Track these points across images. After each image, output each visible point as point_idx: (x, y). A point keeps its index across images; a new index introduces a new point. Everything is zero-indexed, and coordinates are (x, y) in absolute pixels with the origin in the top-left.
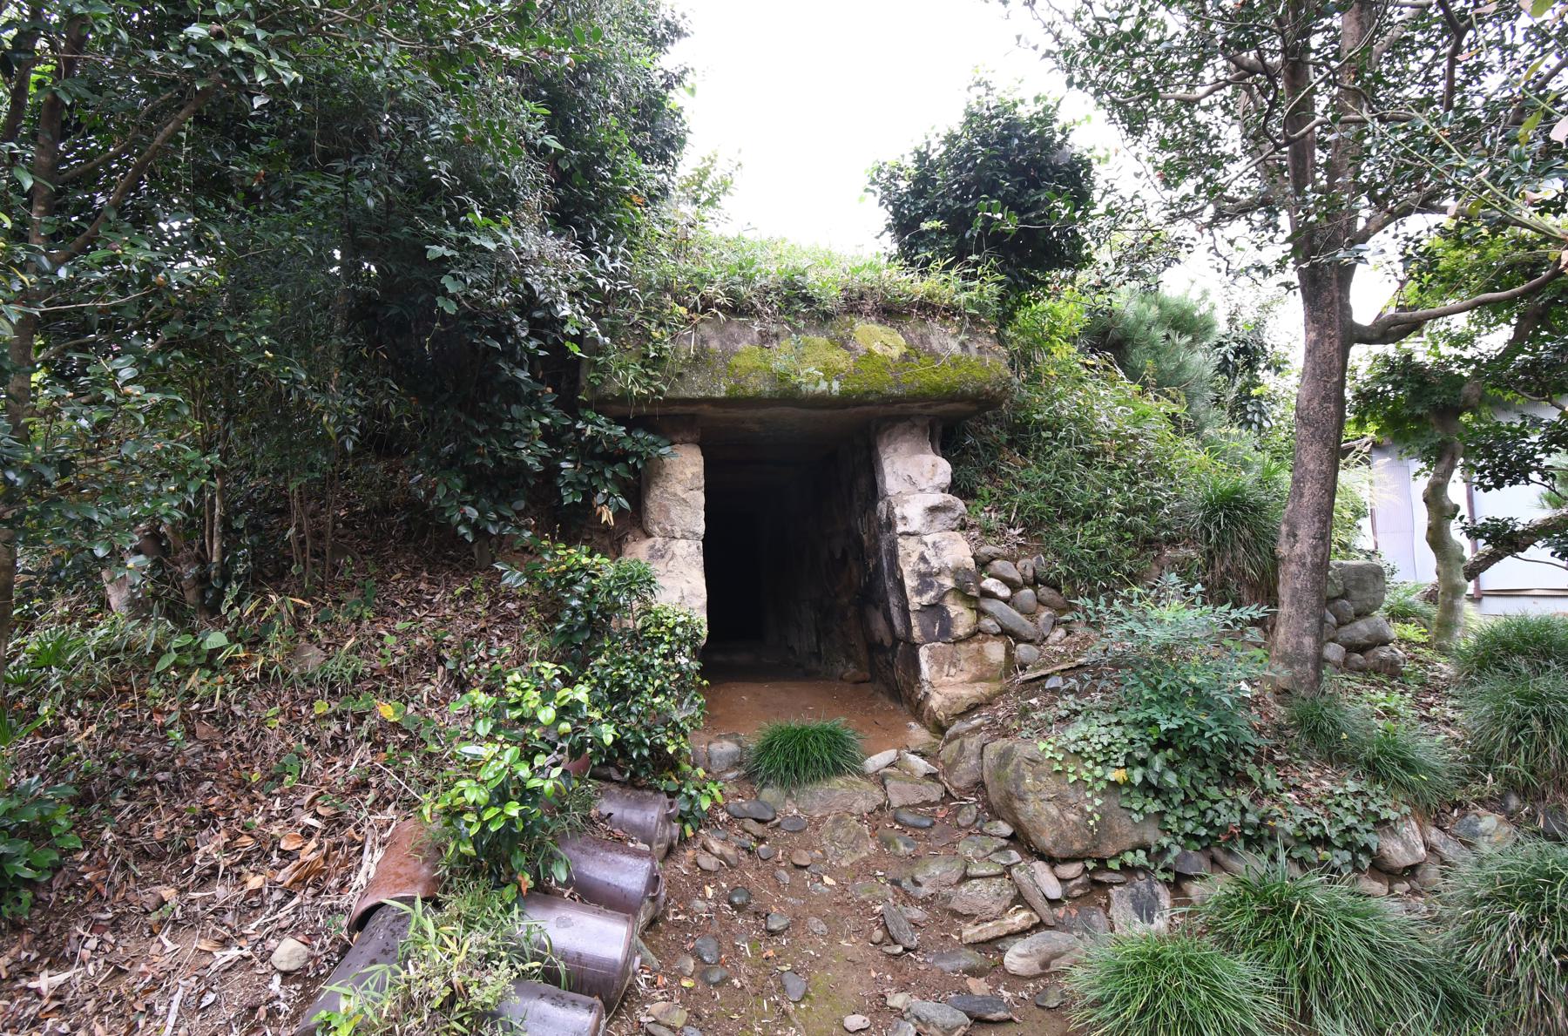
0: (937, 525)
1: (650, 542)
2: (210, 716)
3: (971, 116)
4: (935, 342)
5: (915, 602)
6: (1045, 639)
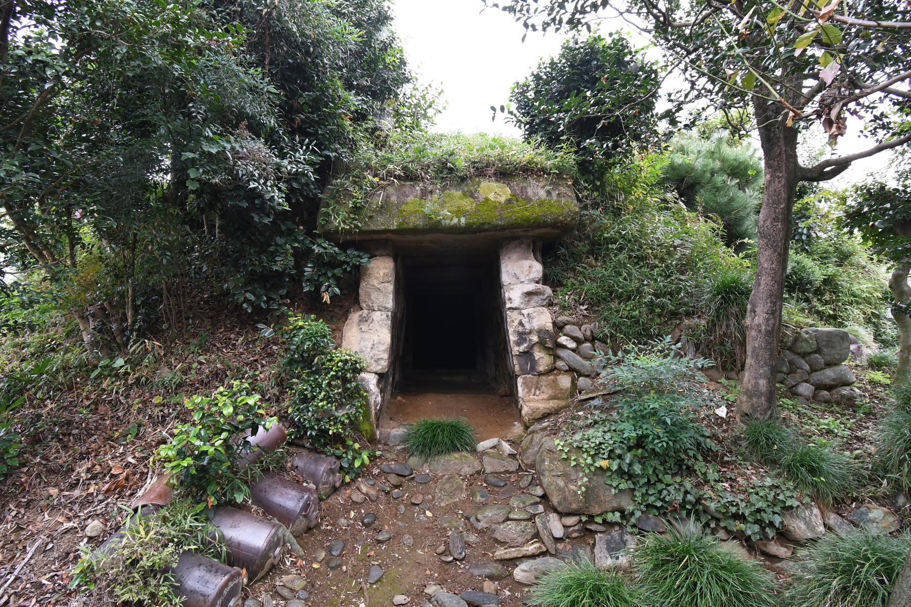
0: (533, 303)
1: (361, 313)
2: (110, 402)
3: (566, 48)
4: (530, 192)
5: (516, 350)
6: (598, 375)
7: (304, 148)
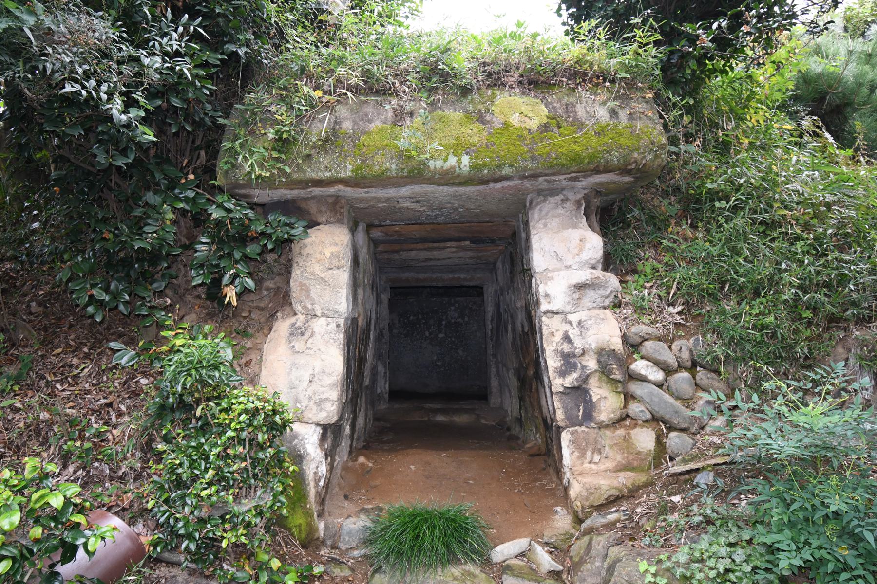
0: (586, 302)
4: (581, 111)
5: (558, 383)
7: (181, 29)
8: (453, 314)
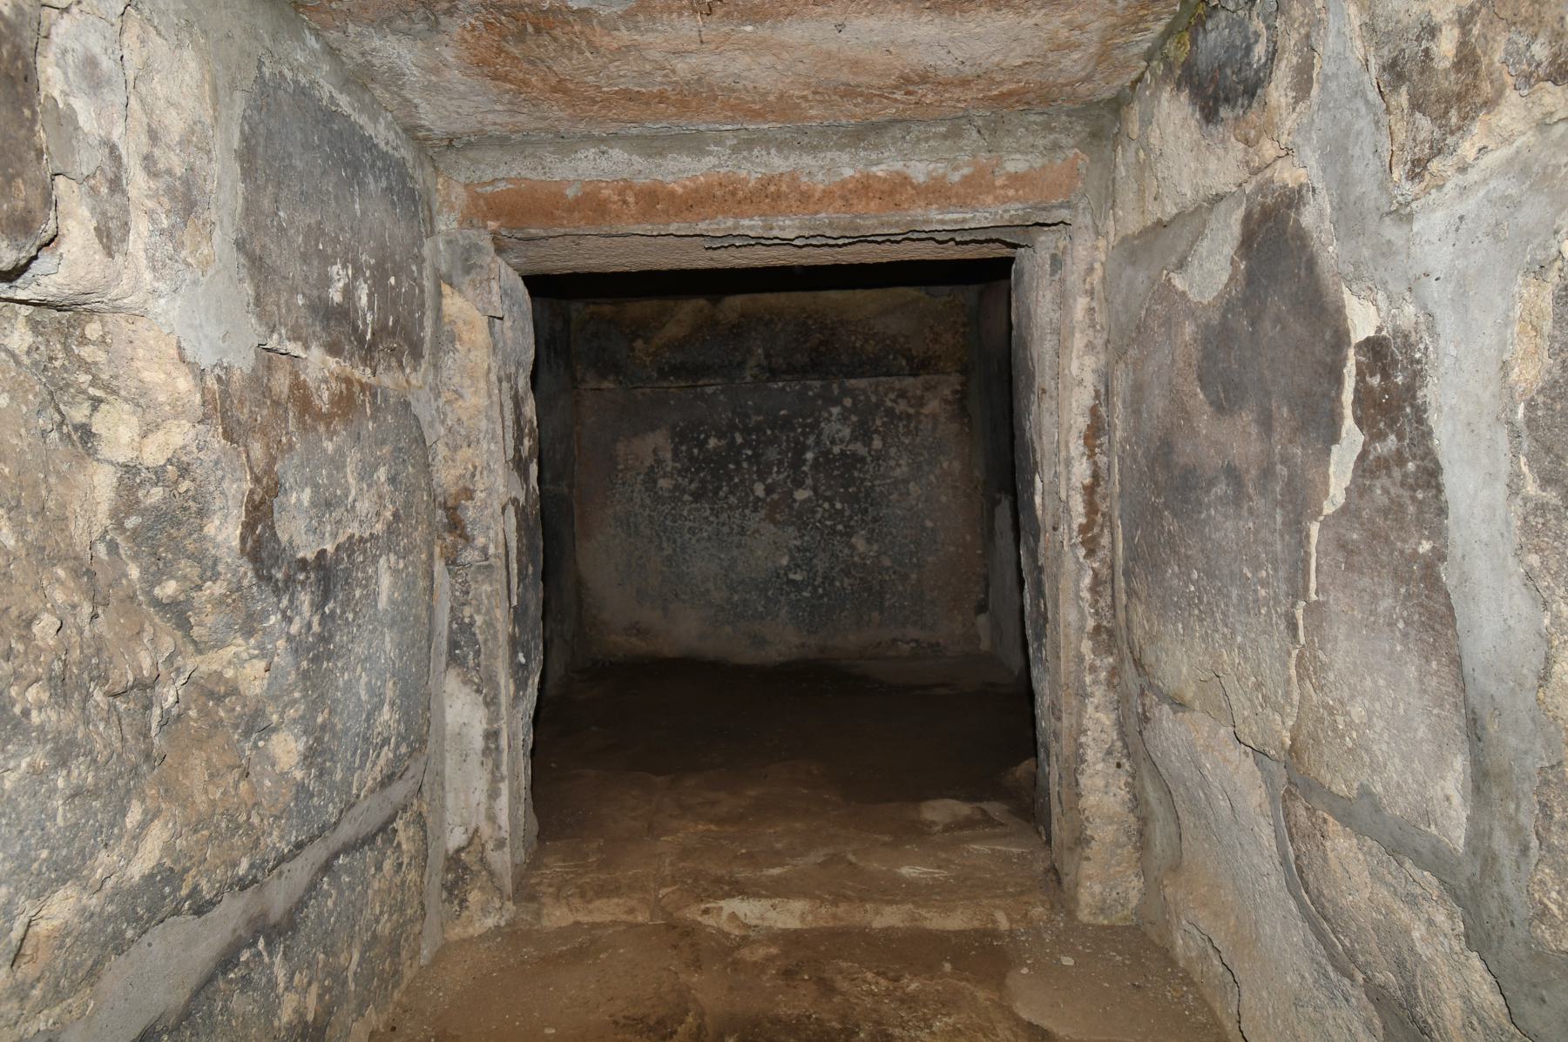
8: (836, 428)
